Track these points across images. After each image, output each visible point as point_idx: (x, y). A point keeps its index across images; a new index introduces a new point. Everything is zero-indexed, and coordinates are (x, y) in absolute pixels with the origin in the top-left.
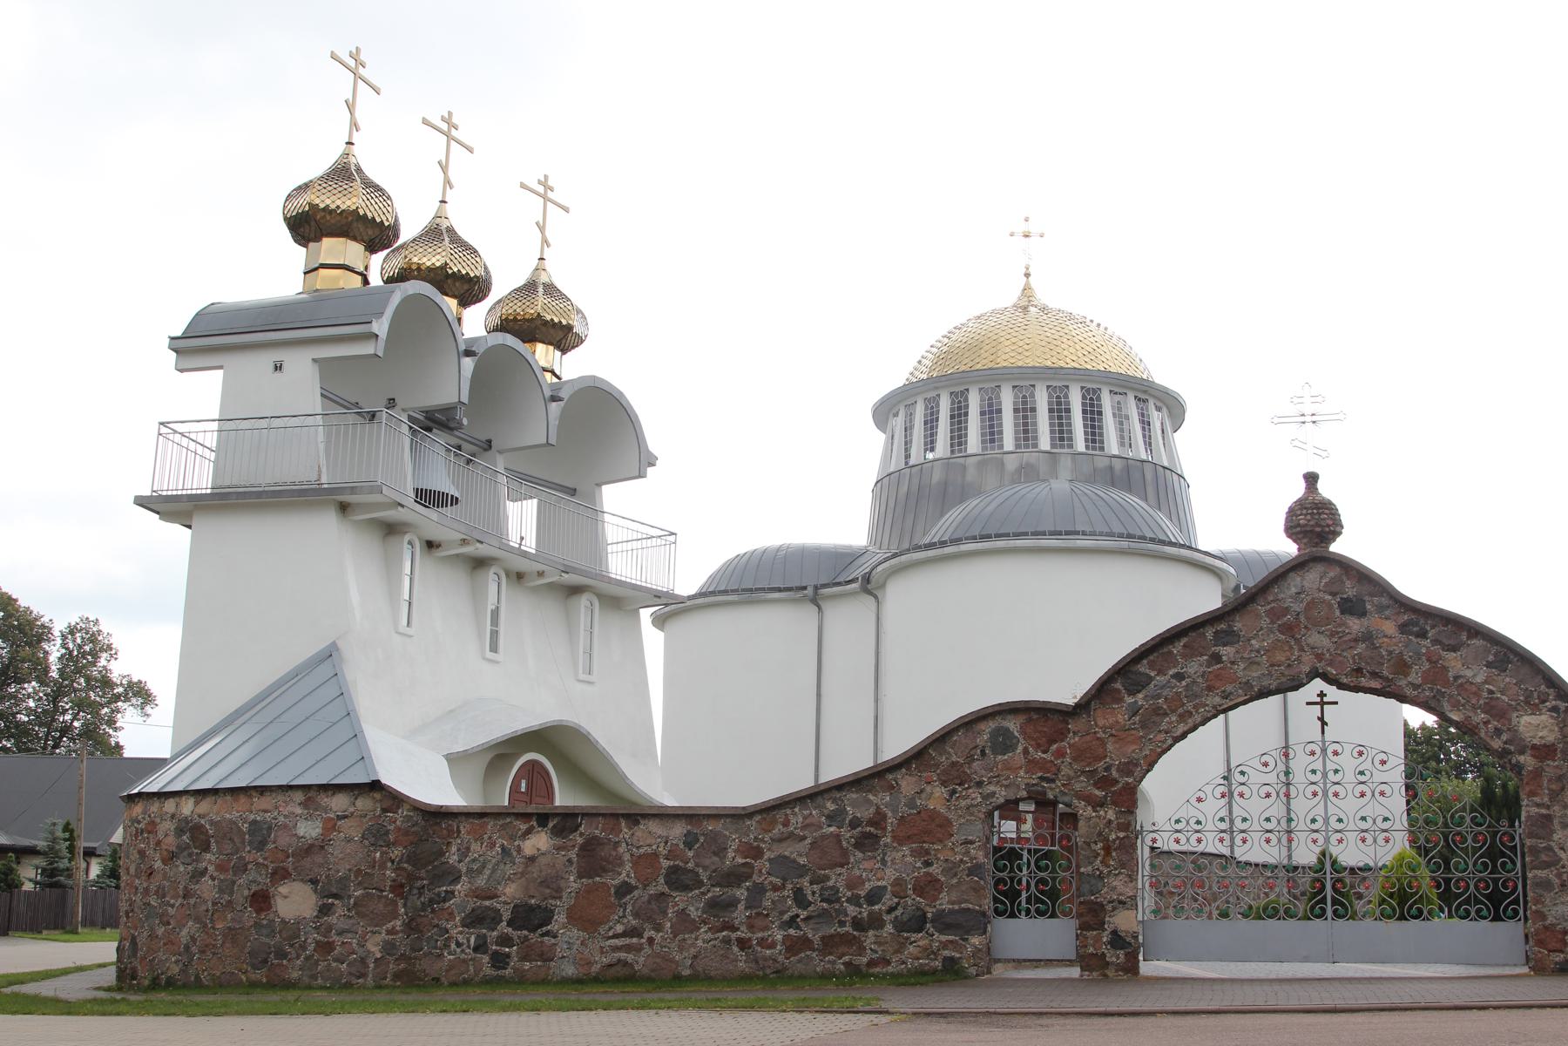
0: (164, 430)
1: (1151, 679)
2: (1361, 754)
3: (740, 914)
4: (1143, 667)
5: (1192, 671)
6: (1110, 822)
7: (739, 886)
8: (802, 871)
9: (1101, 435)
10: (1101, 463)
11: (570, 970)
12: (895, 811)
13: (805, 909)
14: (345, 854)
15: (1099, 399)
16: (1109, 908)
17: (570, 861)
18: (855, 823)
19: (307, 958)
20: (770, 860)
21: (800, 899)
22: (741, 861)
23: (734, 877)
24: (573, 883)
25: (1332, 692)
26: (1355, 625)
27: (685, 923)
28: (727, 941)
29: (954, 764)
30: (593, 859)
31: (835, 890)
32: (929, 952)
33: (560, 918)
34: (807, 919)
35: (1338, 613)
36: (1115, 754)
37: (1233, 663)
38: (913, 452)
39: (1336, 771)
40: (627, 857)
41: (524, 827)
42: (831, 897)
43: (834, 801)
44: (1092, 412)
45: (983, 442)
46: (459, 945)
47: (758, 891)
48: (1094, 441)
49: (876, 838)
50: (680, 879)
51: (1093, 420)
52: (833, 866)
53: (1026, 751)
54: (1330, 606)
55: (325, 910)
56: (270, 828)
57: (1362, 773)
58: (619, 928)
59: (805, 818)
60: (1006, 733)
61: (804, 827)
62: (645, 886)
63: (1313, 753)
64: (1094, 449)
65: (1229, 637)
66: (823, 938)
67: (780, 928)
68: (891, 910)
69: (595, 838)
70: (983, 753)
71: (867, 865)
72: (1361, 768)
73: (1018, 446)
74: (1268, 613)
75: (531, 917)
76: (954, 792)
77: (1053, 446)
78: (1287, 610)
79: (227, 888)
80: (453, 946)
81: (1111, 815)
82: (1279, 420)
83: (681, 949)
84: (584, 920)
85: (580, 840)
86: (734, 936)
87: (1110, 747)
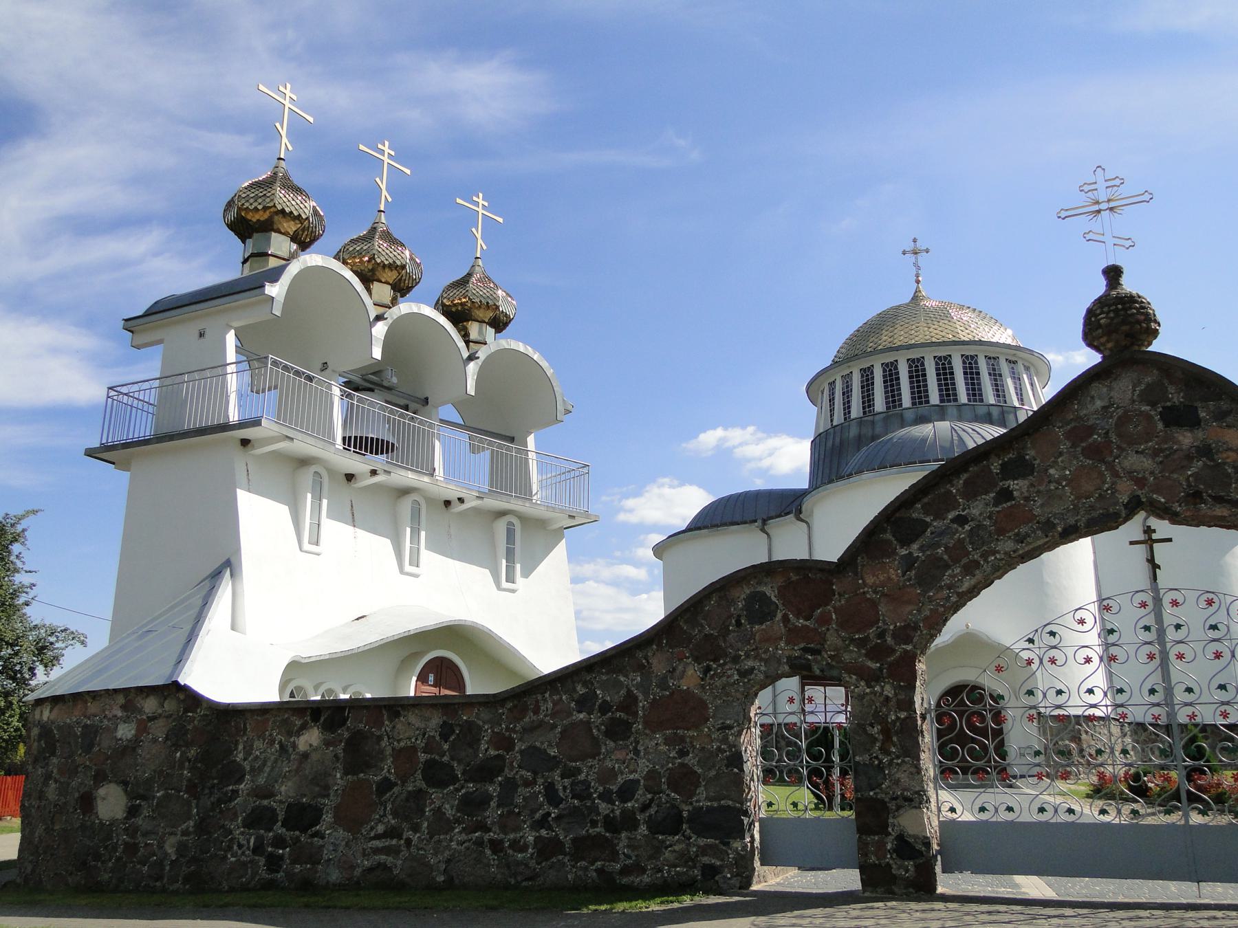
0: (112, 393)
1: (927, 525)
2: (1210, 603)
3: (493, 813)
4: (917, 513)
5: (975, 512)
6: (887, 699)
7: (492, 782)
8: (553, 763)
9: (980, 390)
10: (981, 410)
11: (335, 876)
12: (646, 694)
13: (556, 807)
14: (151, 756)
15: (976, 363)
16: (892, 805)
17: (336, 756)
18: (605, 708)
19: (119, 859)
20: (521, 752)
21: (551, 794)
22: (492, 752)
23: (486, 771)
24: (339, 779)
25: (1162, 527)
26: (1186, 439)
27: (441, 824)
28: (479, 843)
29: (708, 637)
30: (358, 755)
31: (586, 783)
32: (685, 859)
33: (328, 818)
34: (558, 818)
35: (1160, 426)
36: (890, 617)
37: (1027, 499)
38: (835, 417)
39: (1178, 627)
40: (389, 751)
41: (299, 723)
42: (582, 792)
43: (585, 684)
44: (972, 373)
45: (887, 403)
46: (240, 846)
47: (510, 787)
48: (974, 395)
49: (628, 725)
50: (437, 775)
51: (972, 379)
52: (583, 758)
53: (785, 619)
54: (1149, 417)
55: (132, 811)
56: (96, 732)
57: (1214, 627)
58: (381, 828)
59: (555, 704)
60: (763, 598)
61: (553, 715)
62: (404, 783)
63: (1144, 605)
64: (975, 400)
65: (1020, 468)
66: (574, 840)
67: (532, 828)
68: (644, 808)
69: (359, 732)
70: (739, 624)
71: (619, 755)
72: (1212, 622)
73: (914, 404)
74: (1068, 435)
75: (303, 817)
76: (708, 669)
77: (942, 401)
78: (1091, 430)
79: (63, 790)
80: (235, 847)
81: (889, 691)
82: (1065, 215)
83: (435, 854)
84: (350, 820)
85: (346, 735)
86: (486, 837)
87: (882, 609)
